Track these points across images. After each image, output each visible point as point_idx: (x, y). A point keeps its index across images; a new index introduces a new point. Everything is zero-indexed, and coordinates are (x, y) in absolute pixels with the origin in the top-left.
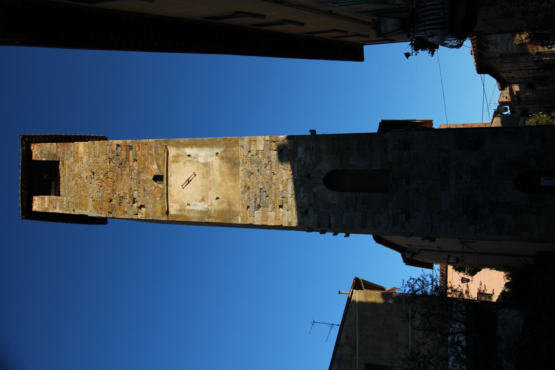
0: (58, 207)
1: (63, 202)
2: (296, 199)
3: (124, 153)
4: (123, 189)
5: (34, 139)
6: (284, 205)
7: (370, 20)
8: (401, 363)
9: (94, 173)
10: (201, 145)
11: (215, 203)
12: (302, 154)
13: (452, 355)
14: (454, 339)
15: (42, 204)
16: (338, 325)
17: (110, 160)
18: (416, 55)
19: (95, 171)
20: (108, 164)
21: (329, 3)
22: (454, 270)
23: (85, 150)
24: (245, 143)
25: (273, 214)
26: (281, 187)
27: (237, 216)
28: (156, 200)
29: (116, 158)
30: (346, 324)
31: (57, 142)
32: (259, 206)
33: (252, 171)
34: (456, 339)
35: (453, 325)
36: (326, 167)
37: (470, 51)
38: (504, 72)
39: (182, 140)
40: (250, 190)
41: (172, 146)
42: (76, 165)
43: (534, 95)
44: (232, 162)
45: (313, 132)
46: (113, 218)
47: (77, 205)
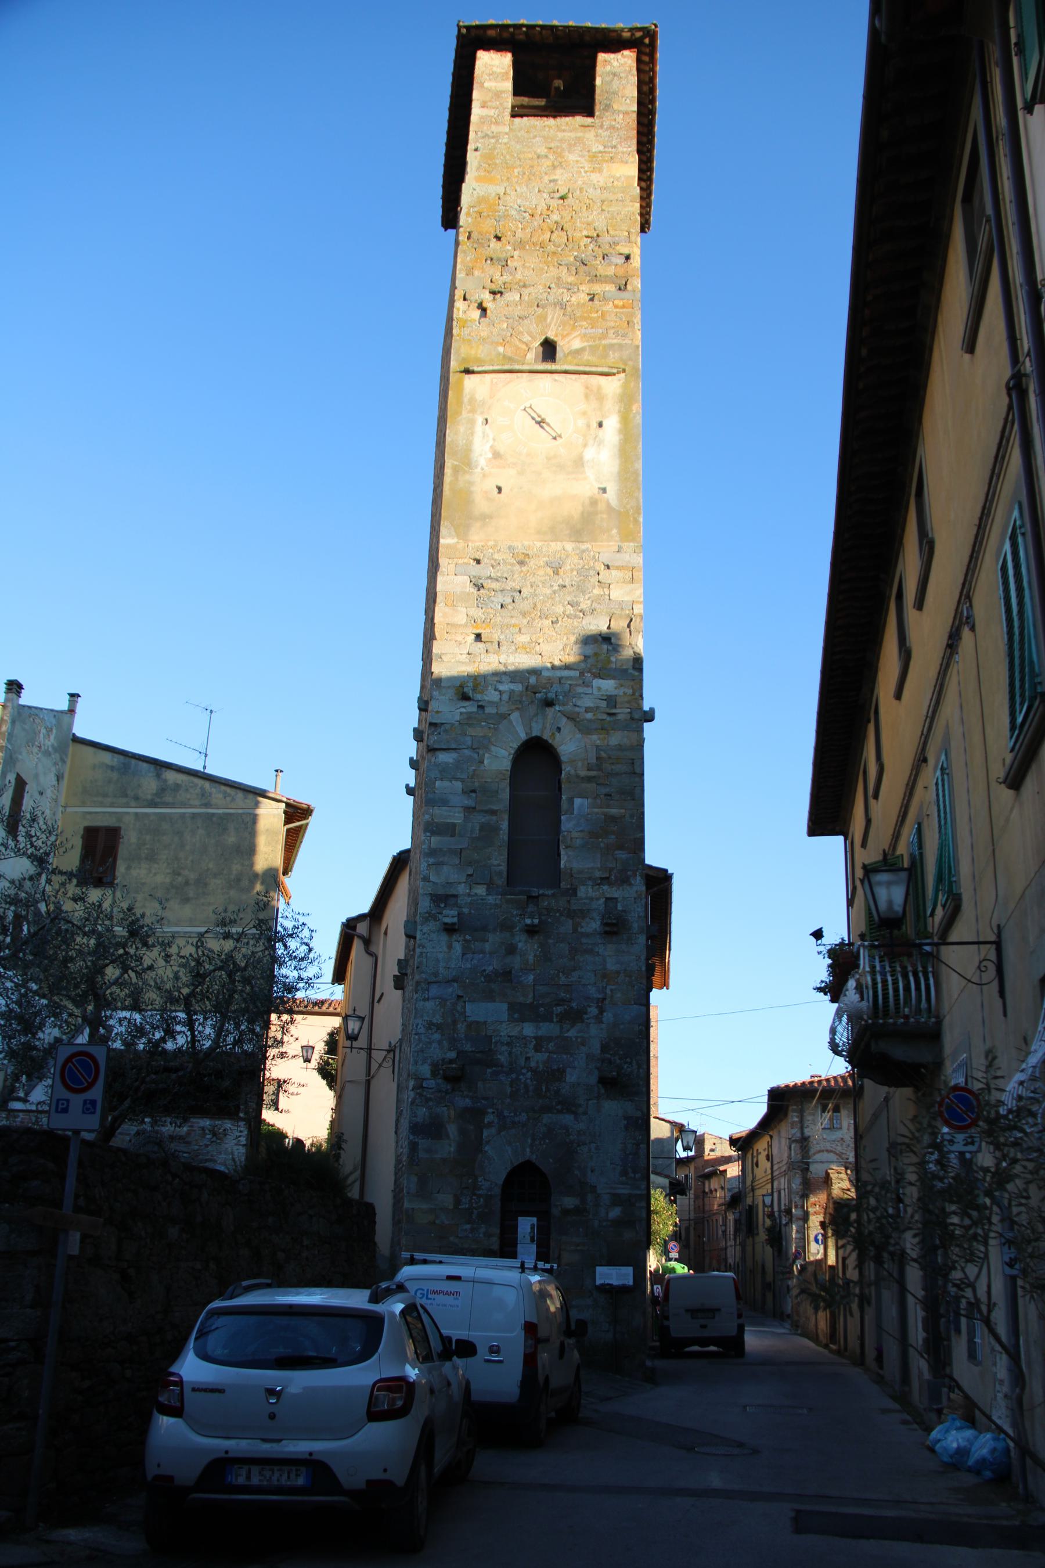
0: (485, 112)
1: (497, 123)
2: (496, 674)
3: (611, 271)
4: (526, 267)
5: (646, 59)
6: (480, 645)
7: (902, 849)
8: (125, 905)
9: (562, 198)
10: (624, 452)
11: (490, 485)
12: (599, 689)
13: (144, 1018)
14: (179, 1023)
15: (493, 73)
16: (205, 767)
17: (595, 238)
18: (819, 953)
19: (570, 201)
20: (585, 233)
21: (943, 757)
22: (329, 1030)
23: (618, 179)
24: (627, 557)
25: (461, 618)
26: (523, 639)
27: (458, 536)
28: (498, 344)
29: (599, 253)
30: (207, 785)
31: (639, 113)
32: (479, 587)
33: (561, 571)
34: (178, 1028)
35: (209, 1022)
36: (569, 745)
37: (819, 1073)
38: (770, 1146)
39: (637, 408)
40: (517, 567)
41: (625, 386)
42: (582, 156)
43: (716, 1207)
44: (583, 526)
45: (649, 716)
46: (457, 244)
47: (489, 157)
